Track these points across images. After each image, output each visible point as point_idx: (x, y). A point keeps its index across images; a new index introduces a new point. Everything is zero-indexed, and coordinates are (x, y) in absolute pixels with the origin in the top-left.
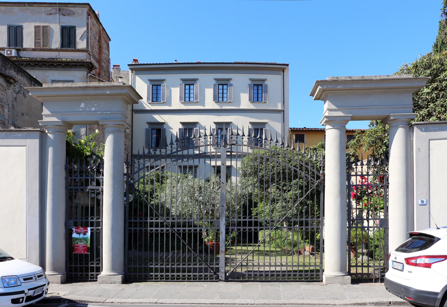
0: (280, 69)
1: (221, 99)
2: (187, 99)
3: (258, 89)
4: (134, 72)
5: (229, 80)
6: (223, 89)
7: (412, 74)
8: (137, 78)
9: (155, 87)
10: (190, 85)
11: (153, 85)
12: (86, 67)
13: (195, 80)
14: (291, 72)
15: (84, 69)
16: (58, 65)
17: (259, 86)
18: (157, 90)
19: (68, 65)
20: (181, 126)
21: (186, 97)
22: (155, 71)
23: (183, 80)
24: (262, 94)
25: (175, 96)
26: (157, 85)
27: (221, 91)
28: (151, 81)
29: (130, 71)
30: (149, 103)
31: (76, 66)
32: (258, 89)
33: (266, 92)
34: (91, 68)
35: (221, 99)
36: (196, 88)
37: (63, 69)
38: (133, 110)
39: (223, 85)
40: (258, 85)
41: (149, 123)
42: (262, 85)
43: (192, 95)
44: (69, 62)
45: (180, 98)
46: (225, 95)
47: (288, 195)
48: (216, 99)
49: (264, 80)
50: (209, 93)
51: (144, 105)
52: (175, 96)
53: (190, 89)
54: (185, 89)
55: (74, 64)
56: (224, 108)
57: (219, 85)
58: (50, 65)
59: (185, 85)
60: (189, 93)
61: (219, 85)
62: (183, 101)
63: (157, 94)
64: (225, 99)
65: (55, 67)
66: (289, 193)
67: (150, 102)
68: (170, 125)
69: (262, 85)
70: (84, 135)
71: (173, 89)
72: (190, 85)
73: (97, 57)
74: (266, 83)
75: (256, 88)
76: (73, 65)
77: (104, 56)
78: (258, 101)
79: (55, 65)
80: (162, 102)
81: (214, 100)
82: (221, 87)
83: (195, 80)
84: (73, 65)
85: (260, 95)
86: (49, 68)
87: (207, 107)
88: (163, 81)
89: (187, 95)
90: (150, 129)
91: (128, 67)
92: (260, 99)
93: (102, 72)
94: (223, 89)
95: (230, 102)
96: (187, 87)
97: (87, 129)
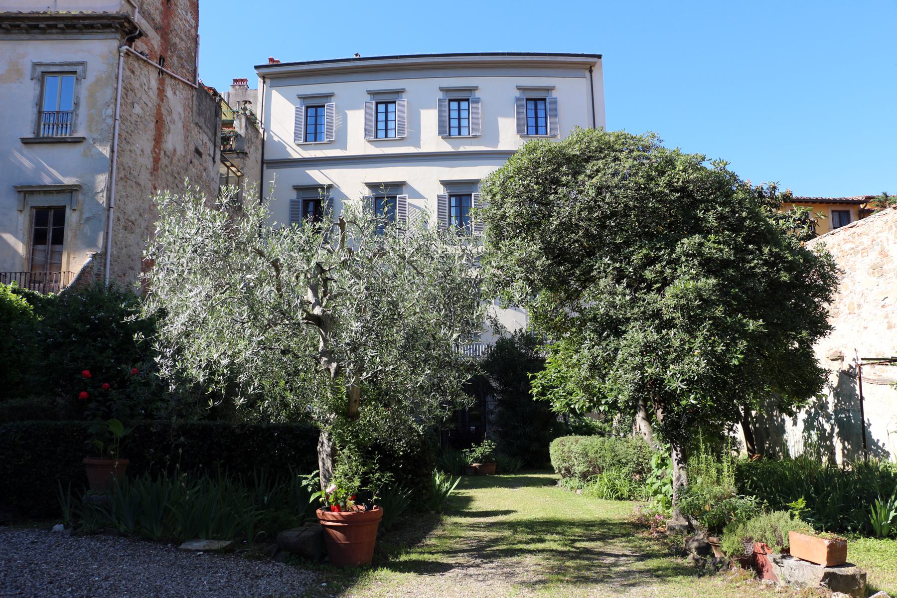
0: (585, 65)
1: (454, 131)
2: (381, 134)
3: (536, 110)
4: (268, 81)
5: (472, 90)
6: (459, 110)
7: (534, 393)
8: (275, 94)
9: (311, 112)
10: (386, 103)
11: (307, 107)
12: (116, 28)
13: (399, 92)
14: (606, 71)
15: (113, 35)
16: (50, 27)
17: (539, 102)
18: (316, 116)
19: (73, 27)
20: (367, 192)
21: (378, 129)
22: (310, 79)
23: (372, 93)
24: (546, 118)
25: (354, 129)
26: (316, 107)
27: (454, 114)
28: (303, 98)
29: (261, 80)
30: (298, 145)
31: (92, 27)
32: (536, 110)
33: (555, 114)
34: (131, 32)
35: (454, 131)
36: (400, 110)
37: (62, 37)
38: (263, 162)
39: (459, 101)
40: (536, 100)
41: (297, 188)
42: (544, 100)
43: (391, 125)
44: (75, 18)
45: (367, 132)
46: (464, 123)
47: (666, 301)
48: (445, 131)
49: (549, 89)
50: (429, 119)
51: (288, 149)
52: (354, 129)
53: (386, 112)
54: (377, 113)
55: (87, 22)
56: (462, 149)
57: (450, 100)
58: (29, 26)
59: (377, 103)
60: (386, 121)
61: (450, 100)
62: (372, 138)
63: (316, 125)
64: (464, 132)
65: (43, 31)
66: (669, 291)
67: (301, 142)
68: (344, 190)
69: (544, 100)
70: (102, 191)
71: (350, 113)
72: (386, 103)
73: (158, 18)
74: (554, 94)
75: (531, 105)
76: (86, 27)
77: (179, 23)
78: (537, 133)
79: (42, 26)
80: (326, 140)
81: (439, 134)
82: (454, 105)
83: (399, 92)
84: (86, 27)
85: (541, 122)
86: (27, 37)
87: (425, 148)
88: (328, 96)
89: (381, 125)
90: (301, 200)
91: (256, 71)
92: (541, 130)
93: (171, 57)
94: (459, 110)
95: (475, 137)
96: (381, 108)
97: (111, 177)
